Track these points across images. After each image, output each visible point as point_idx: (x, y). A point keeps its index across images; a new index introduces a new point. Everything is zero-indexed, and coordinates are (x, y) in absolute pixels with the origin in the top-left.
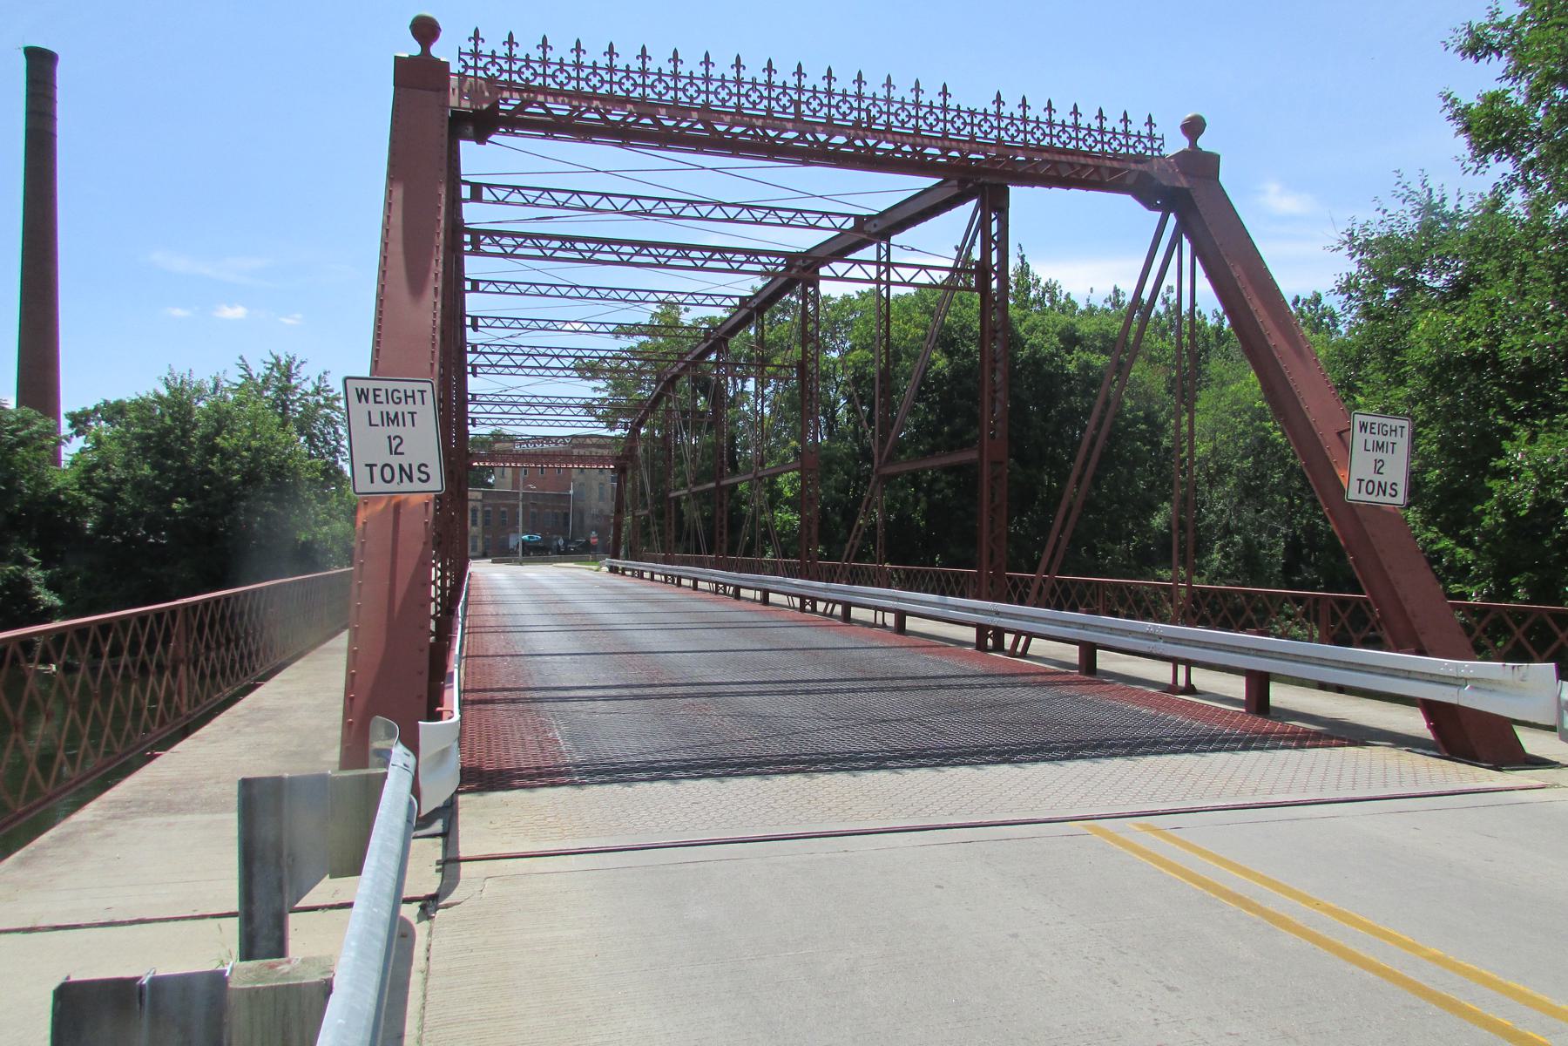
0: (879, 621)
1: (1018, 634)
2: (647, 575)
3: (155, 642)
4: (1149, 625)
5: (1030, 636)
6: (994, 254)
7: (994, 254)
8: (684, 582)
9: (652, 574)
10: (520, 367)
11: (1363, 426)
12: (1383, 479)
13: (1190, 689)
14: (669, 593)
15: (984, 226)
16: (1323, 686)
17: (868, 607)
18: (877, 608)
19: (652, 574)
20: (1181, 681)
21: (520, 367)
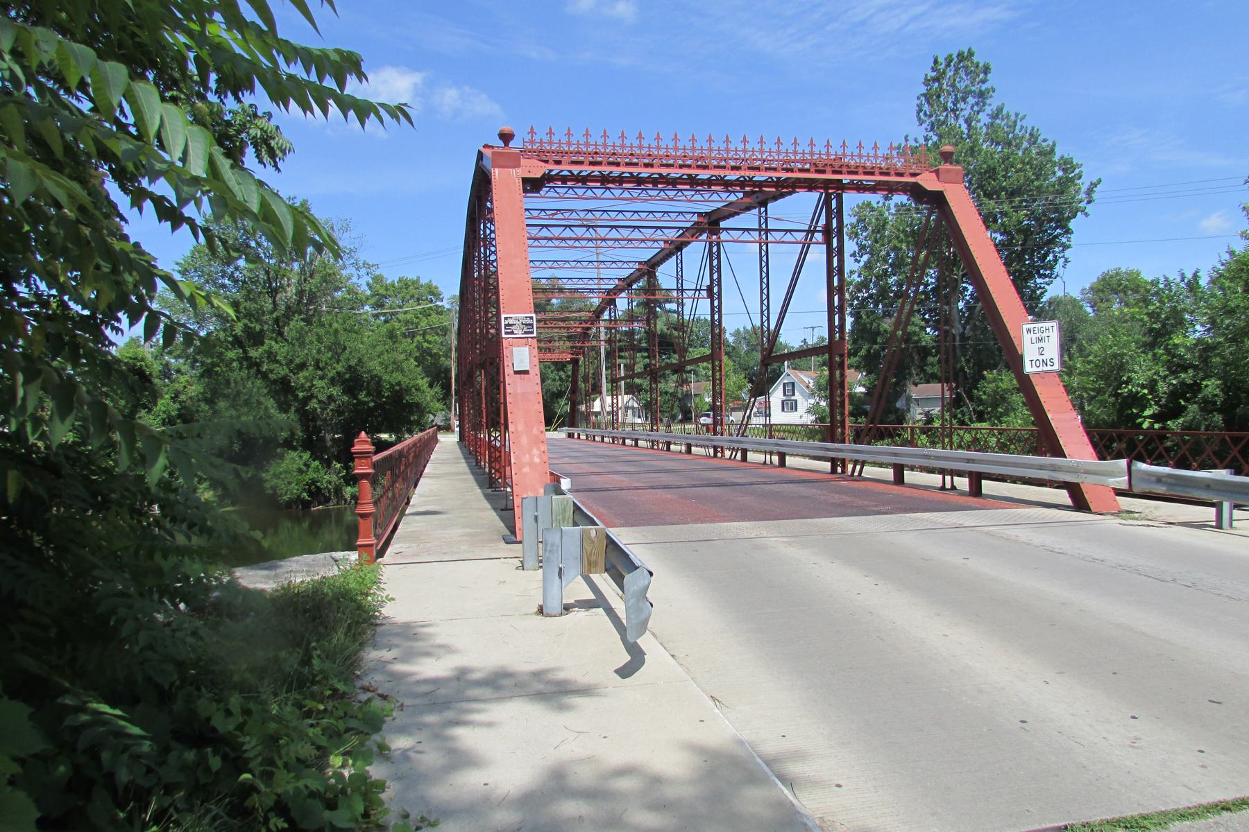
0: (768, 461)
1: (856, 462)
2: (597, 439)
3: (294, 240)
4: (837, 445)
5: (863, 464)
6: (834, 221)
7: (834, 221)
8: (628, 442)
9: (603, 438)
10: (603, 240)
11: (1029, 331)
12: (1044, 357)
13: (860, 478)
14: (618, 451)
15: (827, 202)
16: (803, 456)
17: (760, 452)
18: (943, 472)
19: (603, 438)
20: (948, 486)
21: (603, 240)
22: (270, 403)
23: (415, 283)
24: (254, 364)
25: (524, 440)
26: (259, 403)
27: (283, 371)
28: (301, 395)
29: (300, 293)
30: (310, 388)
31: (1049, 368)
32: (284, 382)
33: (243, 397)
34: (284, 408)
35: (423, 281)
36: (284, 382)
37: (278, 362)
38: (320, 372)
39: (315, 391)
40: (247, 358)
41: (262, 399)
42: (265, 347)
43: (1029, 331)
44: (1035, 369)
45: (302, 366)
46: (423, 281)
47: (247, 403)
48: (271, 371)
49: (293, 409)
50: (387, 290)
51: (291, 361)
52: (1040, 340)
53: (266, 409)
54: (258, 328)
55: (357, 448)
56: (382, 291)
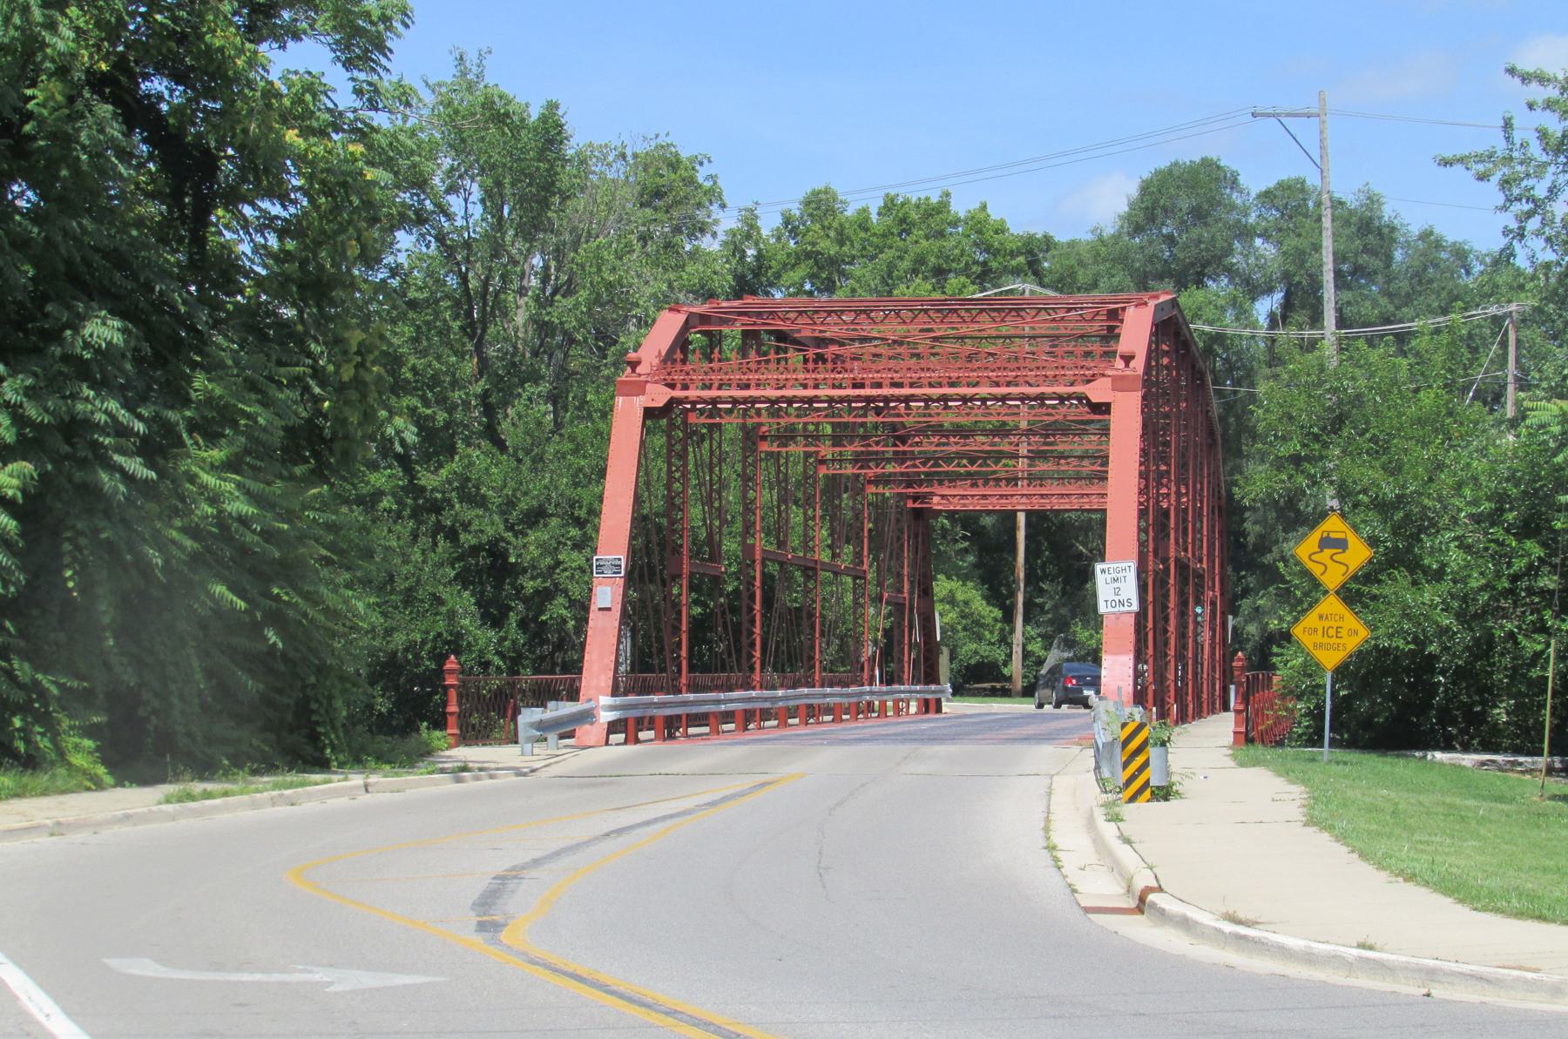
11: (1103, 571)
22: (464, 603)
23: (934, 215)
24: (425, 507)
25: (596, 668)
26: (439, 601)
27: (487, 526)
28: (530, 585)
29: (544, 328)
30: (552, 568)
31: (1126, 609)
32: (496, 551)
33: (401, 585)
34: (493, 615)
35: (960, 207)
36: (496, 551)
37: (482, 502)
38: (574, 532)
39: (562, 577)
40: (417, 490)
41: (445, 593)
42: (455, 465)
43: (1103, 571)
44: (1110, 609)
45: (536, 517)
46: (960, 207)
47: (409, 598)
48: (466, 526)
49: (513, 619)
50: (842, 239)
51: (511, 503)
52: (1116, 580)
53: (452, 615)
54: (442, 416)
55: (448, 666)
56: (828, 247)
